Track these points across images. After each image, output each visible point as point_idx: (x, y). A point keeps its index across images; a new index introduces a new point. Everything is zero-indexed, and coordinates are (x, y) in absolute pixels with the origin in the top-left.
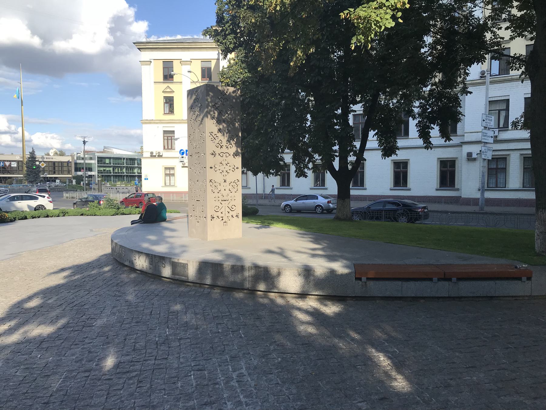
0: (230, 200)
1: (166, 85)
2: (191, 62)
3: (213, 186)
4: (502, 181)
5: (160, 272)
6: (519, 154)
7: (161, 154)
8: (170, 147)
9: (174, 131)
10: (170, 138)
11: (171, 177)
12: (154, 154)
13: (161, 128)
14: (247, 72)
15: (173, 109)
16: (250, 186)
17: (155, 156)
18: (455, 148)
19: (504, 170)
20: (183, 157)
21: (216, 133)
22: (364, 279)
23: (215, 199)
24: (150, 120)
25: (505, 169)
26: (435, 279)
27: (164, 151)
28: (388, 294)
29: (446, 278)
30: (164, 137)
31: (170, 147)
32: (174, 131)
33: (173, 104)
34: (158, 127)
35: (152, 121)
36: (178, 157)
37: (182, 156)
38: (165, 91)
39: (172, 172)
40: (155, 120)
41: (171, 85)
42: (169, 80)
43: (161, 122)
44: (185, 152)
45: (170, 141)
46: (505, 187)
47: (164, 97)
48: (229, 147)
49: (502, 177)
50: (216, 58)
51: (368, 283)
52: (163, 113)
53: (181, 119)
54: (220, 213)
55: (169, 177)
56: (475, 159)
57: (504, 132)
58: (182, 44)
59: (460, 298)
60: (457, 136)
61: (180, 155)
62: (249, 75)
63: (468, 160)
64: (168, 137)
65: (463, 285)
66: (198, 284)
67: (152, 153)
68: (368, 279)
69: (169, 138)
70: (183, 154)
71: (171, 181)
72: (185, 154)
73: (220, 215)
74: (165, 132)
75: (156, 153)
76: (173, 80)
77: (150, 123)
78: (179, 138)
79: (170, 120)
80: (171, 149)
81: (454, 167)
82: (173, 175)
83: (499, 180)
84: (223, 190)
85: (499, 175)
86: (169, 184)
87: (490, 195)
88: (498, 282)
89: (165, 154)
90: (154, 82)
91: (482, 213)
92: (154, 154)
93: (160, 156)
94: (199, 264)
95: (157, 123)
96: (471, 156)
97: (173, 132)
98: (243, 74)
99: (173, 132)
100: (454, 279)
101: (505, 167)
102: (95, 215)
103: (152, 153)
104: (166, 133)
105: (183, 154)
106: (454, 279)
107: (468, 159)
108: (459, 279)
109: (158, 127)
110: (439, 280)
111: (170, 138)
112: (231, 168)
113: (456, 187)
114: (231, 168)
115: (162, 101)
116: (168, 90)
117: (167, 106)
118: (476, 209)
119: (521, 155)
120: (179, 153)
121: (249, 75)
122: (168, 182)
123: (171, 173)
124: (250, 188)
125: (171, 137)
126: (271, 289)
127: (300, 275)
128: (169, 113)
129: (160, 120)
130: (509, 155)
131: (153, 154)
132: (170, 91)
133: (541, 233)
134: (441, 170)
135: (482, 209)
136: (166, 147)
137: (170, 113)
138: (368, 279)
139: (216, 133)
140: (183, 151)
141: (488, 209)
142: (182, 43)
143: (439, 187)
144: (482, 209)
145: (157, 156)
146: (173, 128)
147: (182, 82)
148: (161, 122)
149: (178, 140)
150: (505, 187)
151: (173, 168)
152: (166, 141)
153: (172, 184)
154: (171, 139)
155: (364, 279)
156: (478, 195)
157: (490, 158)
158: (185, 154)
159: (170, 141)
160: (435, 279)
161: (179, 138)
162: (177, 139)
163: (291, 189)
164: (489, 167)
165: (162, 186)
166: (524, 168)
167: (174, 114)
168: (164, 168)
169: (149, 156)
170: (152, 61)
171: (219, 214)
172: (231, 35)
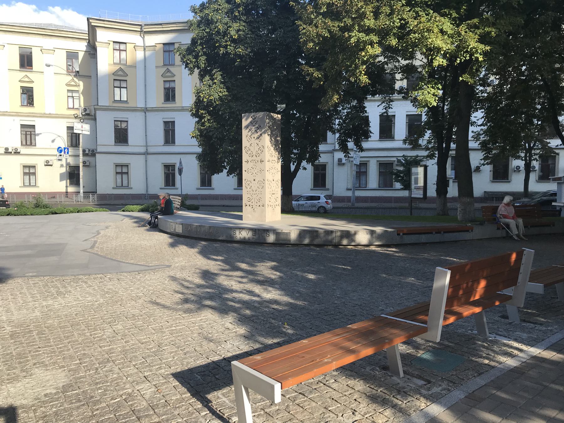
0: (258, 194)
1: (24, 74)
2: (54, 51)
3: (247, 184)
4: (364, 183)
5: (265, 239)
6: (376, 161)
7: (19, 151)
8: (28, 143)
9: (34, 125)
10: (29, 133)
11: (31, 177)
12: (10, 150)
13: (17, 122)
14: (226, 91)
15: (33, 101)
16: (132, 186)
17: (11, 152)
18: (326, 154)
19: (365, 173)
20: (61, 155)
21: (249, 147)
22: (401, 234)
23: (247, 193)
24: (4, 112)
25: (366, 172)
26: (434, 233)
27: (22, 147)
28: (412, 242)
29: (438, 232)
30: (21, 131)
31: (28, 143)
32: (34, 125)
33: (32, 96)
34: (14, 120)
35: (7, 113)
36: (56, 154)
37: (60, 154)
38: (22, 80)
39: (32, 171)
40: (9, 112)
41: (29, 74)
42: (26, 68)
43: (18, 114)
44: (63, 150)
45: (28, 137)
46: (366, 187)
47: (21, 87)
48: (257, 156)
49: (364, 178)
50: (85, 50)
51: (403, 236)
52: (20, 105)
53: (43, 112)
54: (251, 202)
55: (28, 177)
56: (344, 164)
57: (365, 142)
58: (44, 30)
59: (443, 242)
60: (327, 144)
61: (58, 153)
62: (227, 93)
63: (339, 164)
64: (26, 132)
65: (446, 235)
66: (297, 245)
67: (7, 149)
68: (404, 234)
69: (27, 133)
70: (61, 151)
71: (35, 182)
72: (63, 152)
73: (251, 204)
74: (23, 126)
75: (13, 150)
76: (32, 69)
77: (4, 115)
78: (41, 134)
79: (30, 113)
80: (31, 144)
81: (325, 170)
82: (34, 174)
83: (361, 182)
84: (272, 187)
85: (361, 177)
86: (28, 184)
87: (359, 193)
88: (460, 233)
89: (23, 150)
90: (9, 70)
91: (353, 208)
92: (10, 150)
93: (17, 153)
94: (300, 232)
95: (13, 116)
96: (341, 161)
97: (33, 126)
98: (222, 93)
99: (33, 126)
100: (442, 232)
101: (366, 171)
102: (24, 215)
103: (7, 149)
104: (23, 128)
105: (61, 151)
106: (442, 232)
107: (339, 164)
108: (445, 232)
109: (14, 120)
110: (436, 233)
111: (29, 133)
112: (250, 171)
113: (327, 187)
114: (250, 171)
115: (19, 91)
116: (26, 79)
117: (25, 96)
118: (350, 204)
119: (378, 161)
120: (57, 150)
121: (227, 93)
122: (119, 180)
123: (31, 171)
124: (132, 188)
125: (31, 132)
126: (350, 243)
127: (367, 234)
128: (27, 106)
129: (17, 113)
130: (368, 161)
131: (8, 150)
132: (28, 80)
133: (462, 210)
134: (314, 173)
135: (353, 204)
136: (24, 143)
137: (29, 105)
138: (404, 234)
139: (249, 147)
140: (61, 149)
141: (357, 205)
142: (44, 29)
143: (313, 187)
144: (353, 204)
145: (13, 153)
146: (34, 122)
147: (43, 72)
148: (18, 114)
149: (40, 135)
150: (366, 187)
151: (34, 167)
152: (24, 137)
153: (33, 185)
154: (31, 135)
155: (401, 234)
156: (349, 194)
157: (358, 164)
158: (63, 152)
159: (28, 137)
160: (434, 233)
161: (41, 134)
162: (38, 135)
163: (213, 189)
164: (380, 171)
165: (20, 186)
166: (380, 172)
167: (33, 107)
168: (22, 167)
169: (3, 153)
170: (6, 45)
171: (250, 203)
172: (203, 57)
